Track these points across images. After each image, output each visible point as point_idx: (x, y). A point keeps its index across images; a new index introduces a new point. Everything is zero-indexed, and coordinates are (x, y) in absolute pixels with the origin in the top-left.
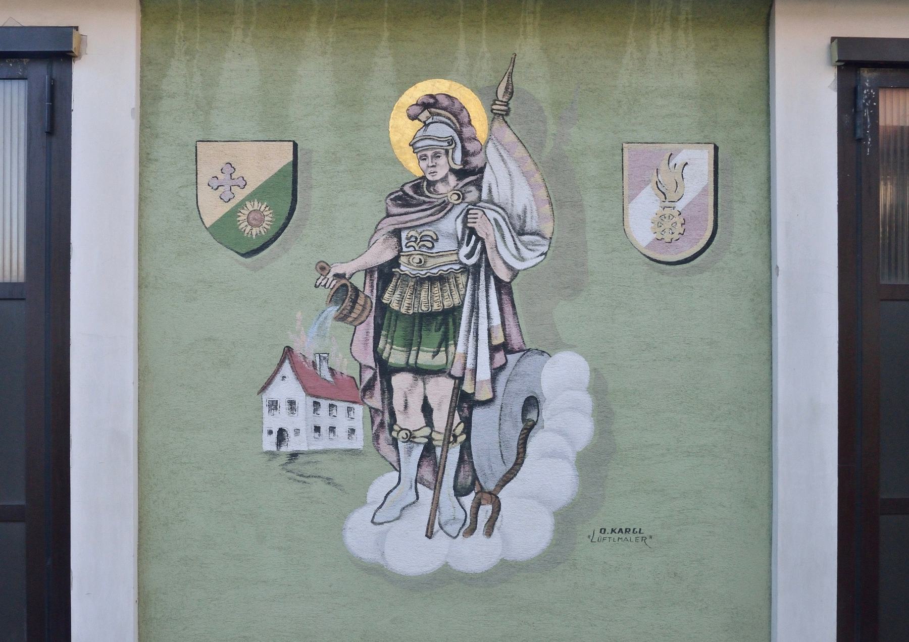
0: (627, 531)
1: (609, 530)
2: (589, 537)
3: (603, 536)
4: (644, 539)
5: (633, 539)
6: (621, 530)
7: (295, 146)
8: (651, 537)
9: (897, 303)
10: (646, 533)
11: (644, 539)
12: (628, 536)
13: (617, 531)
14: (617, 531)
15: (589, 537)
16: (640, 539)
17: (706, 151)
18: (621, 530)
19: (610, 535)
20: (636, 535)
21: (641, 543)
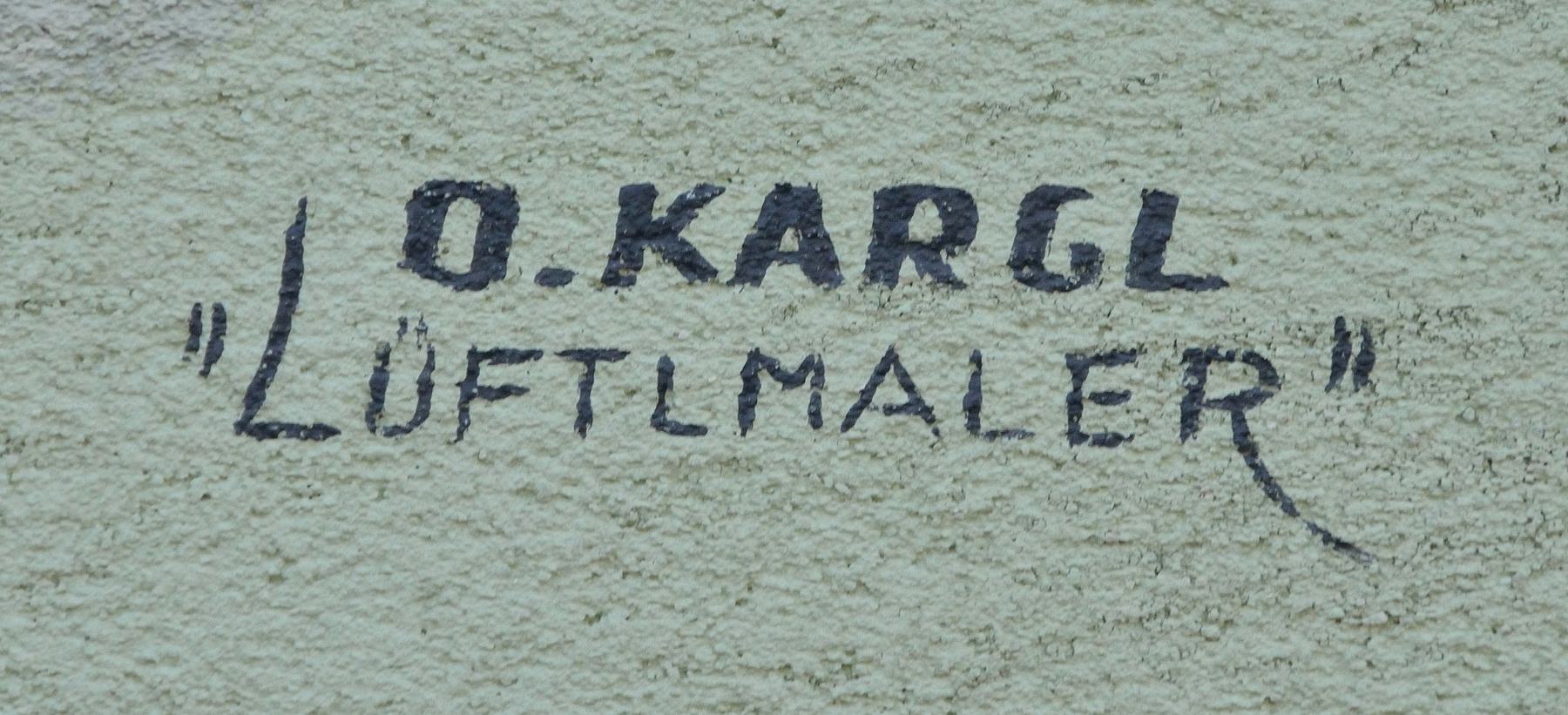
0: (916, 231)
1: (568, 220)
2: (205, 334)
3: (463, 321)
4: (1223, 390)
5: (1028, 386)
6: (793, 209)
7: (976, 360)
8: (1353, 357)
9: (272, 309)
10: (1271, 293)
11: (1223, 390)
12: (931, 327)
13: (720, 233)
14: (720, 233)
15: (205, 334)
16: (1154, 391)
17: (572, 370)
18: (793, 209)
19: (593, 315)
20: (1082, 316)
21: (1170, 470)
